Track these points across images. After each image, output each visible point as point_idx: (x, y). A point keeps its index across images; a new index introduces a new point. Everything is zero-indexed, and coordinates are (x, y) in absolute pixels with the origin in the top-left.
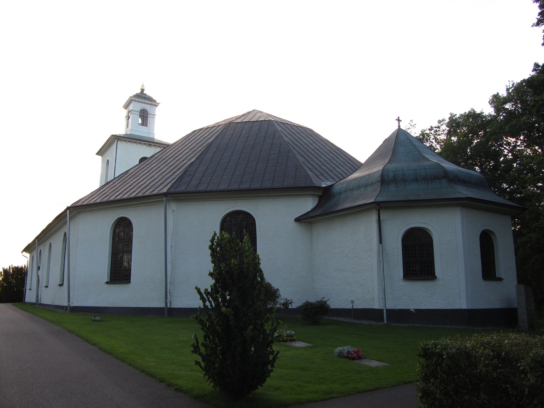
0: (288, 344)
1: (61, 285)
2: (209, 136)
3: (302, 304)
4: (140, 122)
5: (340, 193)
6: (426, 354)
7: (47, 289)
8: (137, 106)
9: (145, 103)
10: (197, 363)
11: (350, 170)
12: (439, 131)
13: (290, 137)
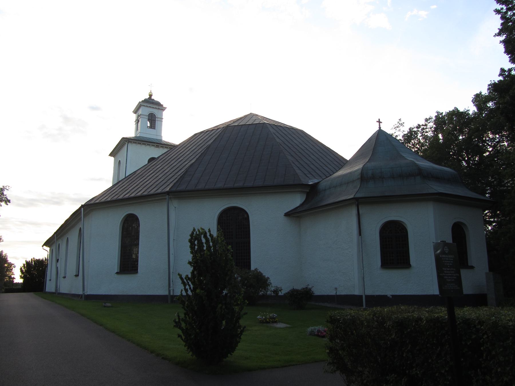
0: (268, 325)
1: (77, 276)
2: (209, 139)
3: (288, 291)
4: (149, 125)
5: (325, 190)
6: (332, 321)
7: (66, 279)
8: (146, 111)
9: (153, 108)
10: (179, 336)
11: (336, 168)
12: (426, 128)
13: (282, 139)
